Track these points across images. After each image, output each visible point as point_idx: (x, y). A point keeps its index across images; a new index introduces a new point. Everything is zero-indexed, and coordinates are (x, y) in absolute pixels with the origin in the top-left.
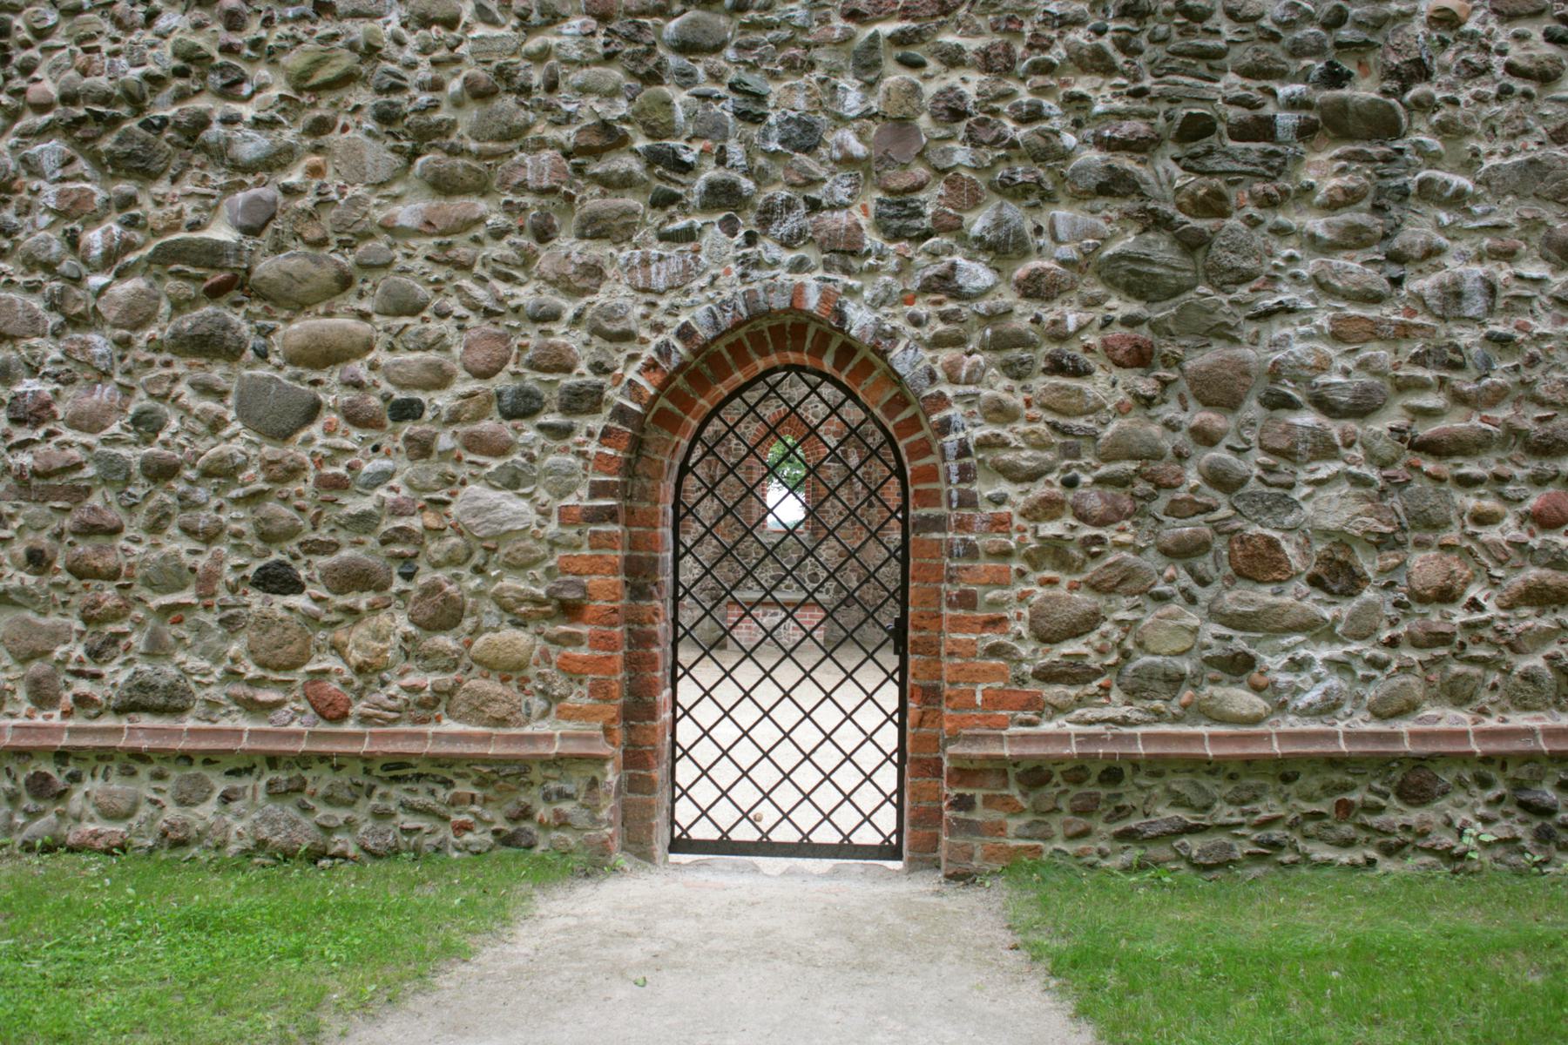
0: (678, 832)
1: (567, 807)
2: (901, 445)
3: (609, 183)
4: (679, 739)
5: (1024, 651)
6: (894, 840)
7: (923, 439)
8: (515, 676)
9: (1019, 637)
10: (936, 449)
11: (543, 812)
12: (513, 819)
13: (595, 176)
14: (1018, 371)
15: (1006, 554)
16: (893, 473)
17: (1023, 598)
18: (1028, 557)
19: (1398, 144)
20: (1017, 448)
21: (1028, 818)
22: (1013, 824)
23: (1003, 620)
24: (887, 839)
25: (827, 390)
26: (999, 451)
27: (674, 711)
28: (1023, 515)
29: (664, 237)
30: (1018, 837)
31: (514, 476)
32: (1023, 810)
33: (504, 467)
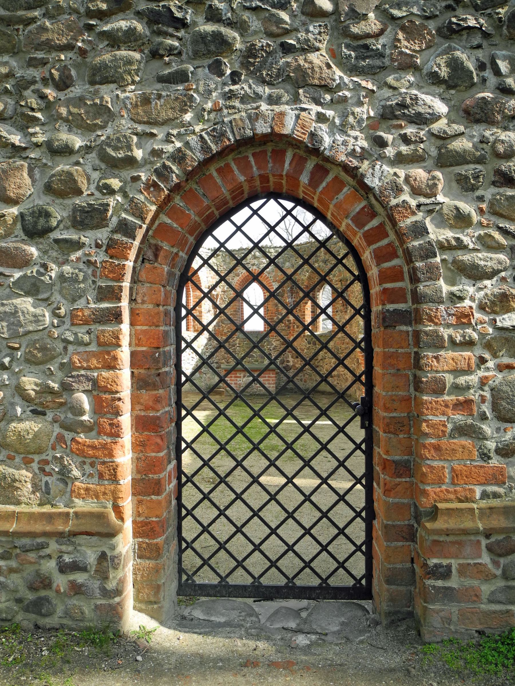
0: (184, 577)
1: (80, 578)
2: (392, 236)
3: (114, 40)
4: (184, 501)
5: (487, 429)
6: (363, 582)
7: (389, 245)
8: (36, 458)
9: (483, 417)
10: (400, 252)
11: (61, 582)
12: (32, 588)
13: (103, 34)
14: (466, 186)
15: (469, 344)
16: (356, 278)
17: (483, 382)
18: (488, 346)
19: (143, 414)
20: (475, 250)
21: (501, 583)
22: (486, 589)
23: (468, 402)
24: (359, 581)
25: (301, 213)
26: (460, 252)
27: (179, 479)
28: (482, 308)
29: (161, 79)
30: (491, 601)
31: (34, 285)
32: (495, 576)
33: (25, 276)
